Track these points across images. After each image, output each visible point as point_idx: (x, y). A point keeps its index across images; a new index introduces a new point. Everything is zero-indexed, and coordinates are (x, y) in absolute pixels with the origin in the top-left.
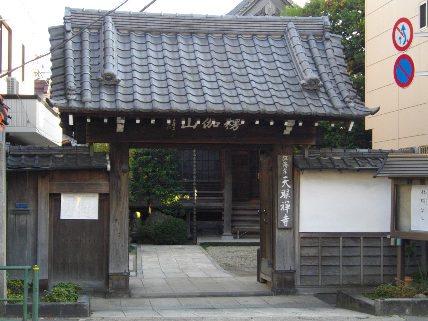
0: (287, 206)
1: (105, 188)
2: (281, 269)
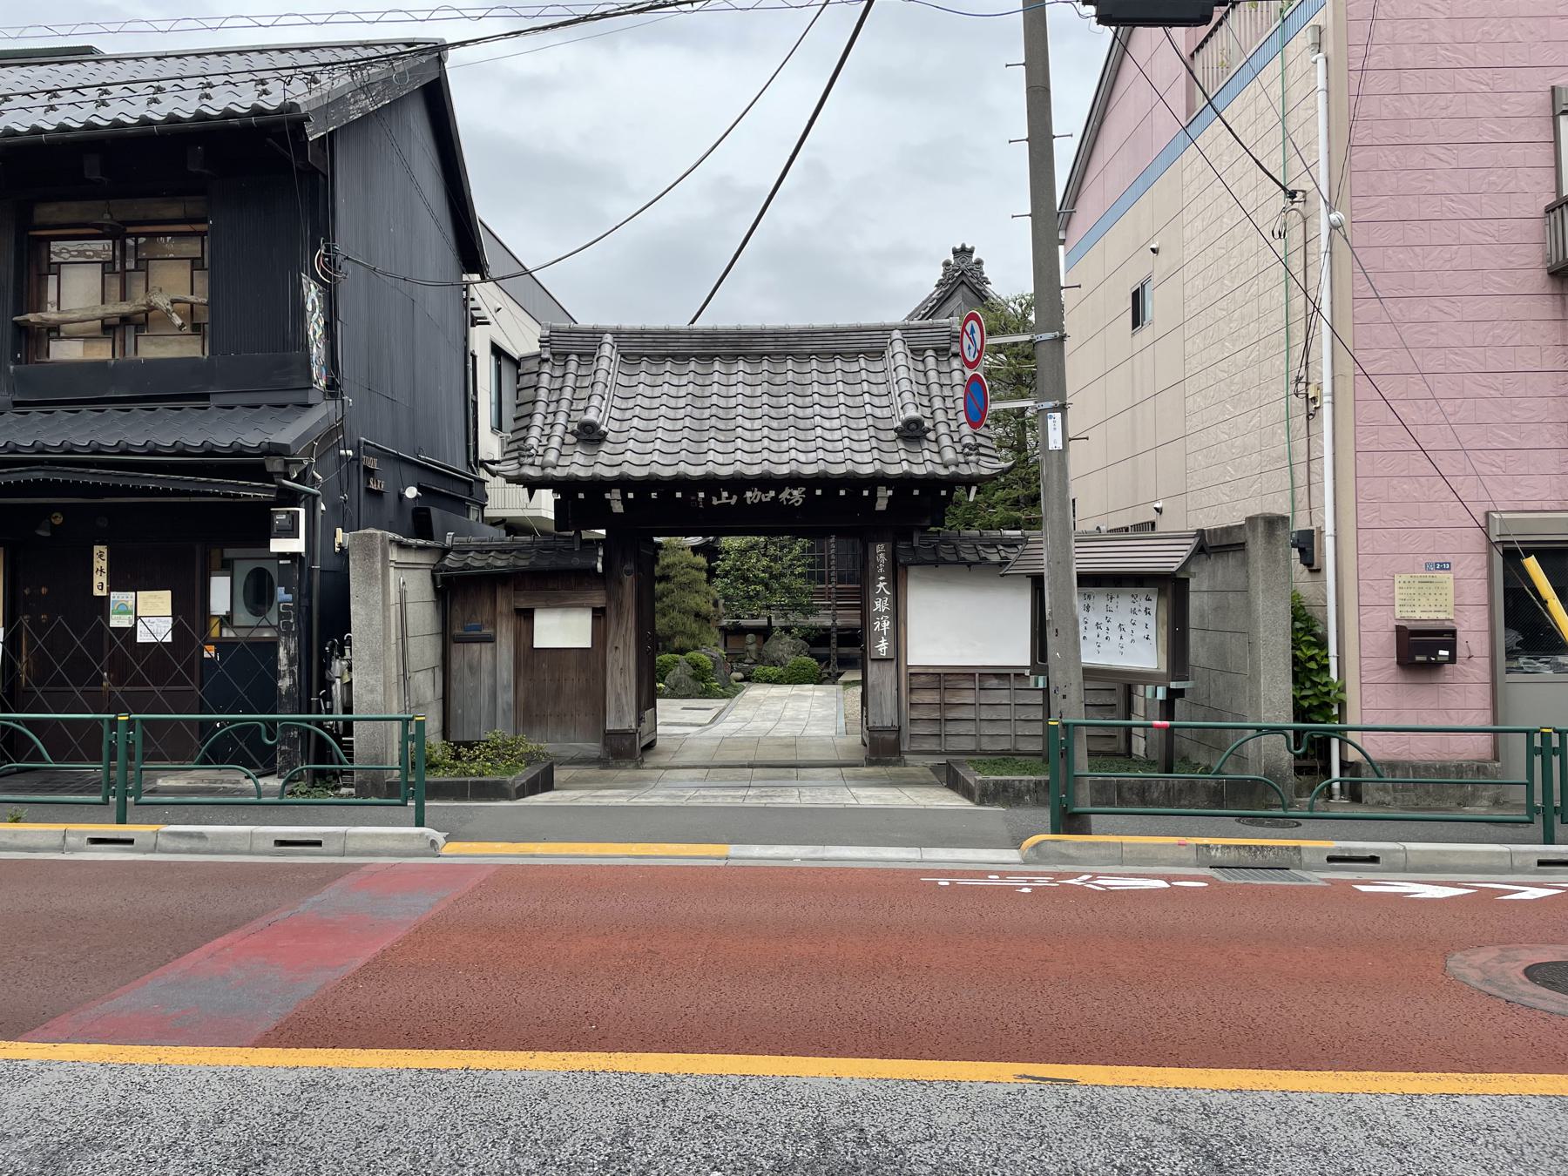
1: (599, 601)
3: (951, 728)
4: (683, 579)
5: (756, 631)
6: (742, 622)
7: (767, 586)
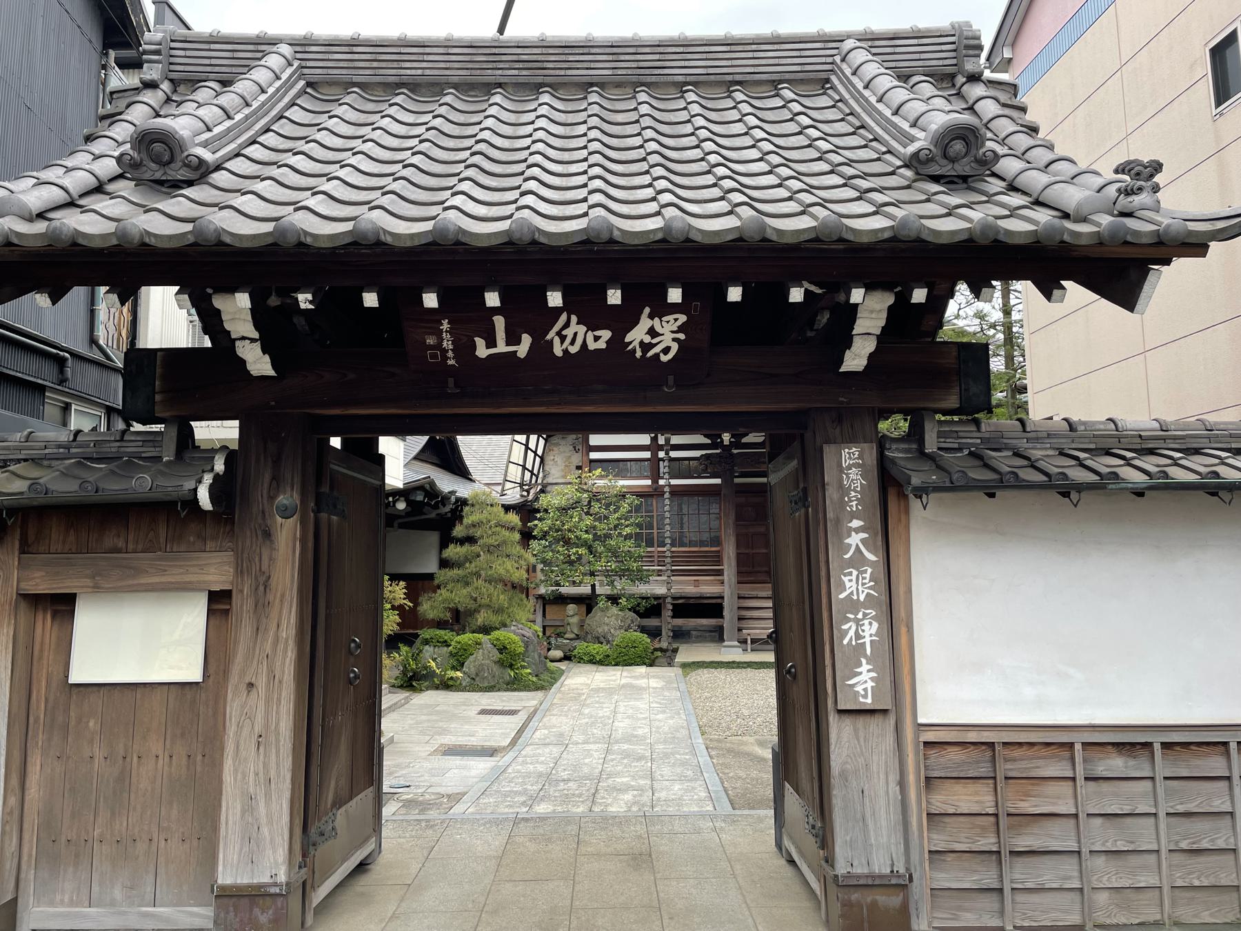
0: (866, 627)
2: (858, 870)
3: (1021, 873)
4: (492, 541)
5: (577, 599)
6: (563, 590)
7: (590, 549)
